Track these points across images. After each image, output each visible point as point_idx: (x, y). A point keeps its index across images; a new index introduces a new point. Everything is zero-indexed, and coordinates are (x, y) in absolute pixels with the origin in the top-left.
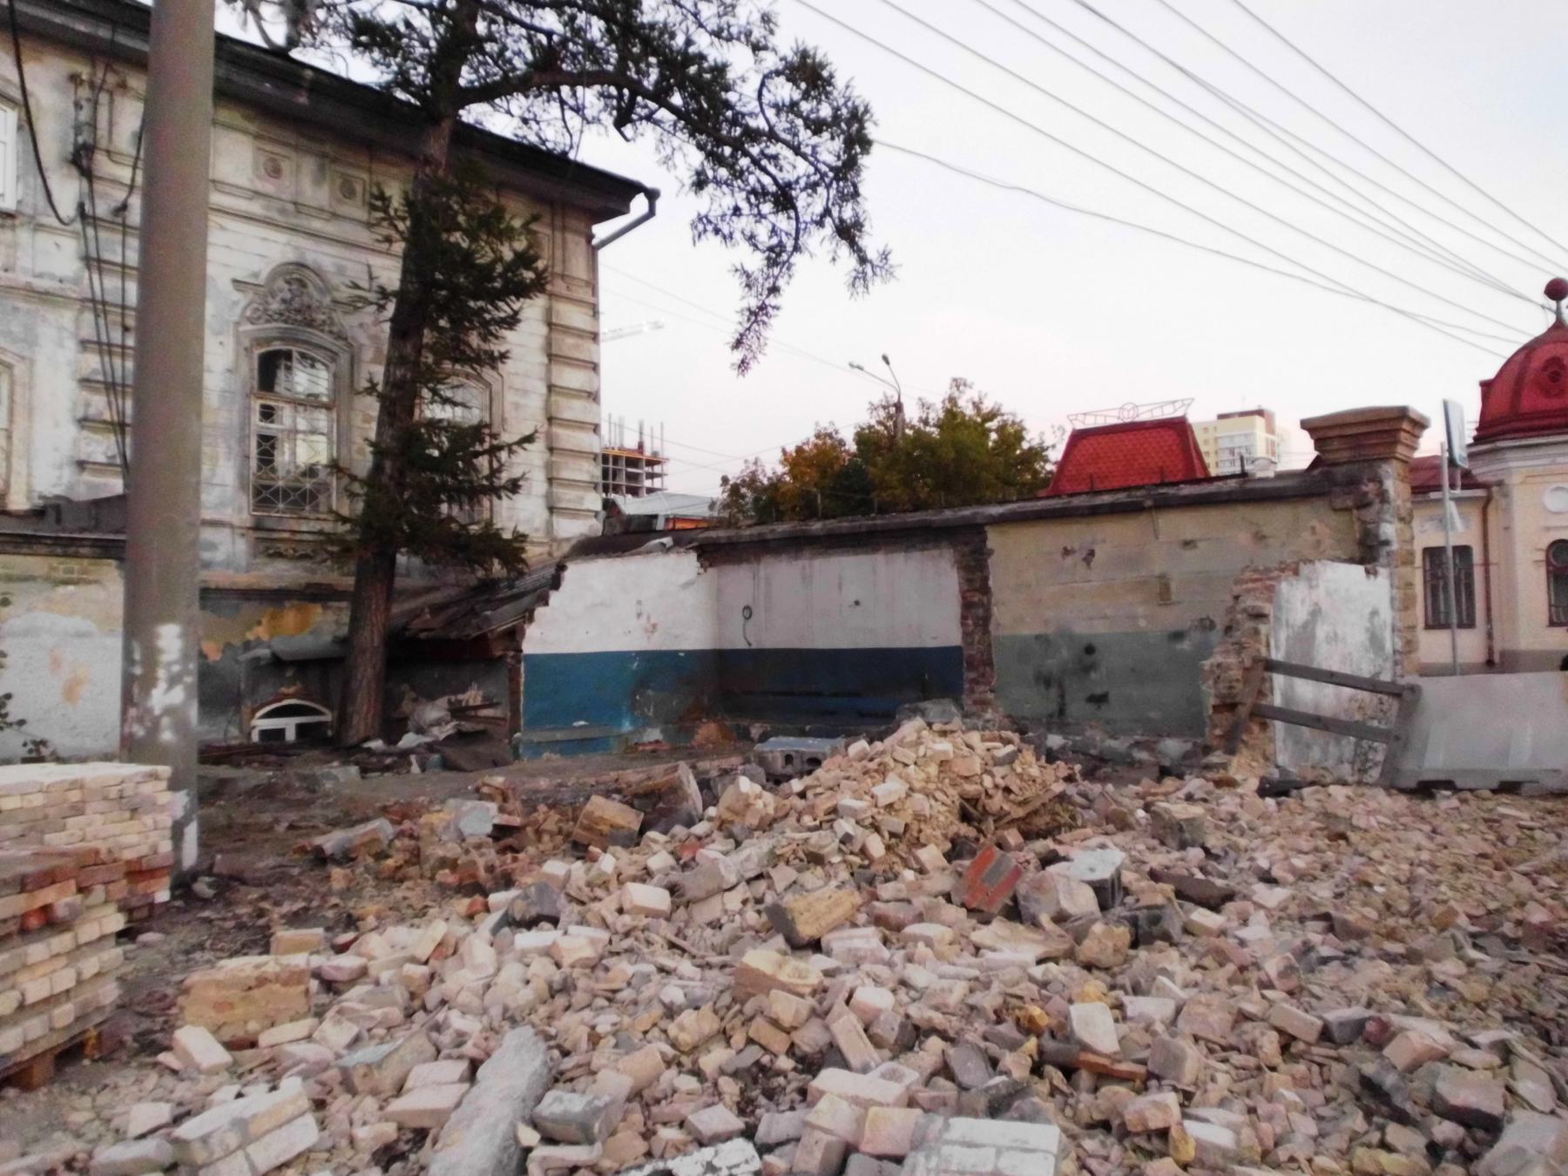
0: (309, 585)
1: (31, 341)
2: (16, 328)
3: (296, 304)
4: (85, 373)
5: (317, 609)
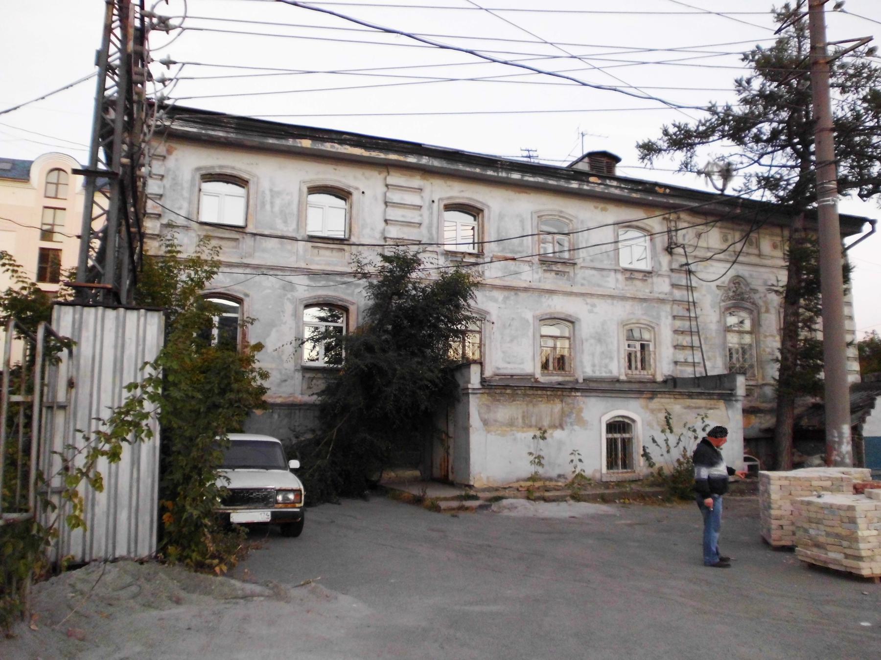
0: (751, 407)
1: (658, 317)
2: (655, 314)
3: (738, 292)
4: (676, 328)
5: (753, 417)
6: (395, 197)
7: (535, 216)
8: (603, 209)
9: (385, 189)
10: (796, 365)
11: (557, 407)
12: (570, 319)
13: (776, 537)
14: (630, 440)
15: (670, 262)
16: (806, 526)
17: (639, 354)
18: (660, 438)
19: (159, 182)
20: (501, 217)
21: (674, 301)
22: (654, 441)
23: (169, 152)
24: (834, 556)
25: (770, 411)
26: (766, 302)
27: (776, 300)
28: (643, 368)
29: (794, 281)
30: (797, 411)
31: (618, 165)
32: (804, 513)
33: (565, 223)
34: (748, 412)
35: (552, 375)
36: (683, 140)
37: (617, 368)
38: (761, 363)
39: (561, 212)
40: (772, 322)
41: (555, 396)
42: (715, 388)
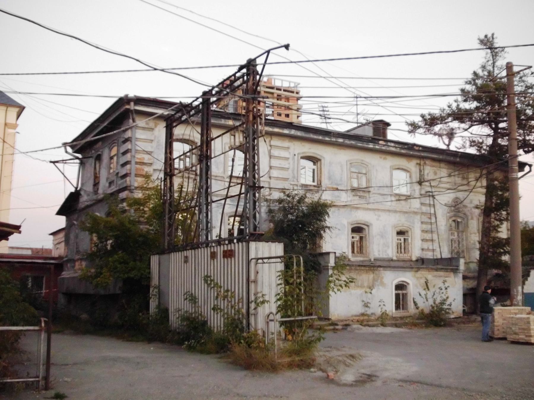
4: (423, 229)
6: (275, 152)
7: (348, 163)
8: (385, 159)
9: (269, 148)
10: (489, 252)
11: (371, 276)
12: (366, 224)
13: (498, 334)
14: (406, 294)
15: (421, 189)
16: (511, 326)
17: (403, 244)
18: (423, 293)
19: (150, 144)
20: (330, 164)
21: (423, 213)
22: (420, 295)
23: (156, 126)
24: (522, 337)
25: (473, 278)
26: (471, 213)
27: (477, 212)
28: (405, 253)
29: (489, 204)
30: (489, 277)
31: (389, 127)
32: (511, 322)
33: (364, 167)
34: (465, 278)
35: (356, 257)
36: (431, 121)
37: (391, 253)
38: (468, 250)
39: (362, 160)
40: (475, 226)
41: (371, 270)
42: (448, 265)
